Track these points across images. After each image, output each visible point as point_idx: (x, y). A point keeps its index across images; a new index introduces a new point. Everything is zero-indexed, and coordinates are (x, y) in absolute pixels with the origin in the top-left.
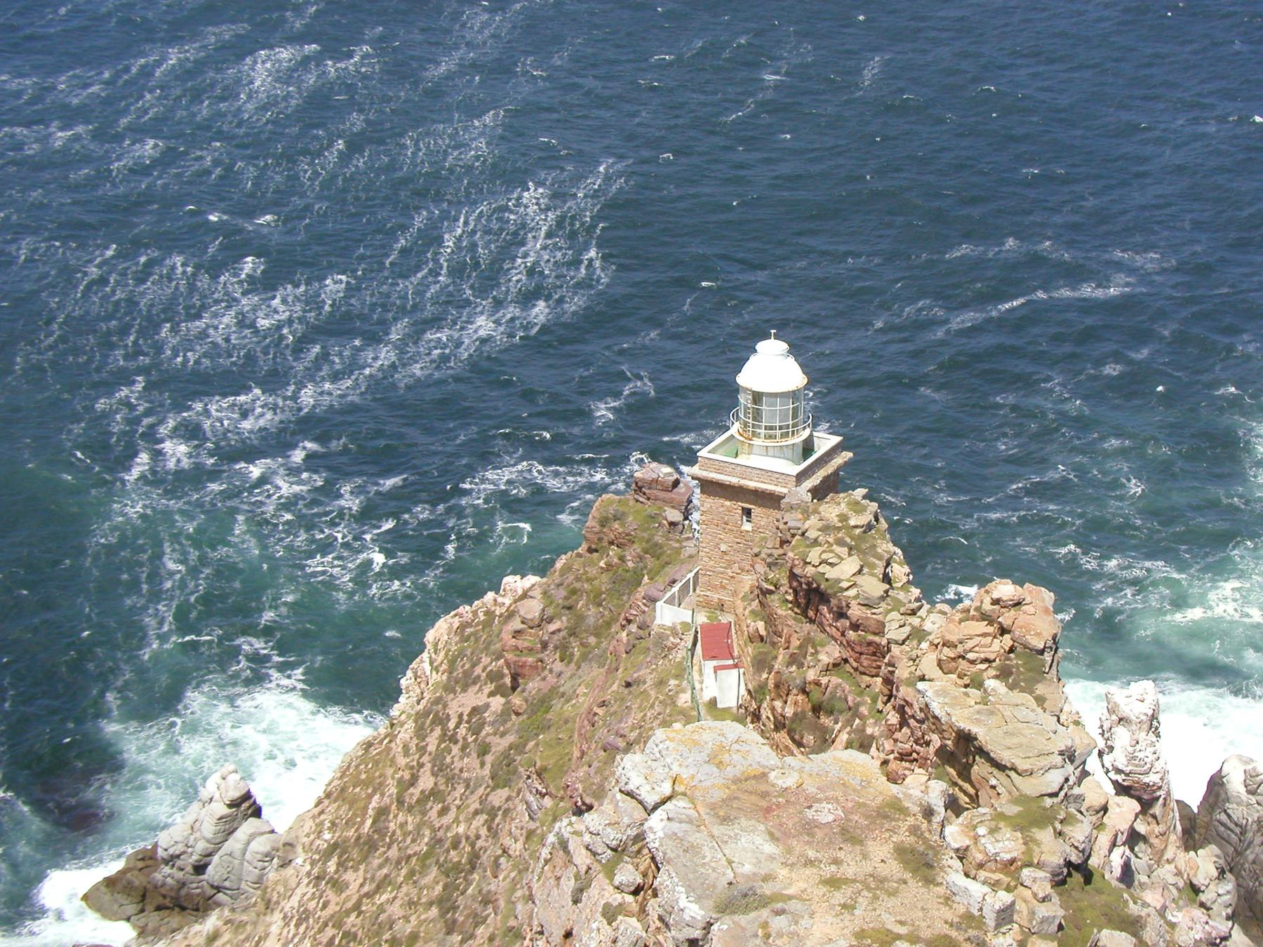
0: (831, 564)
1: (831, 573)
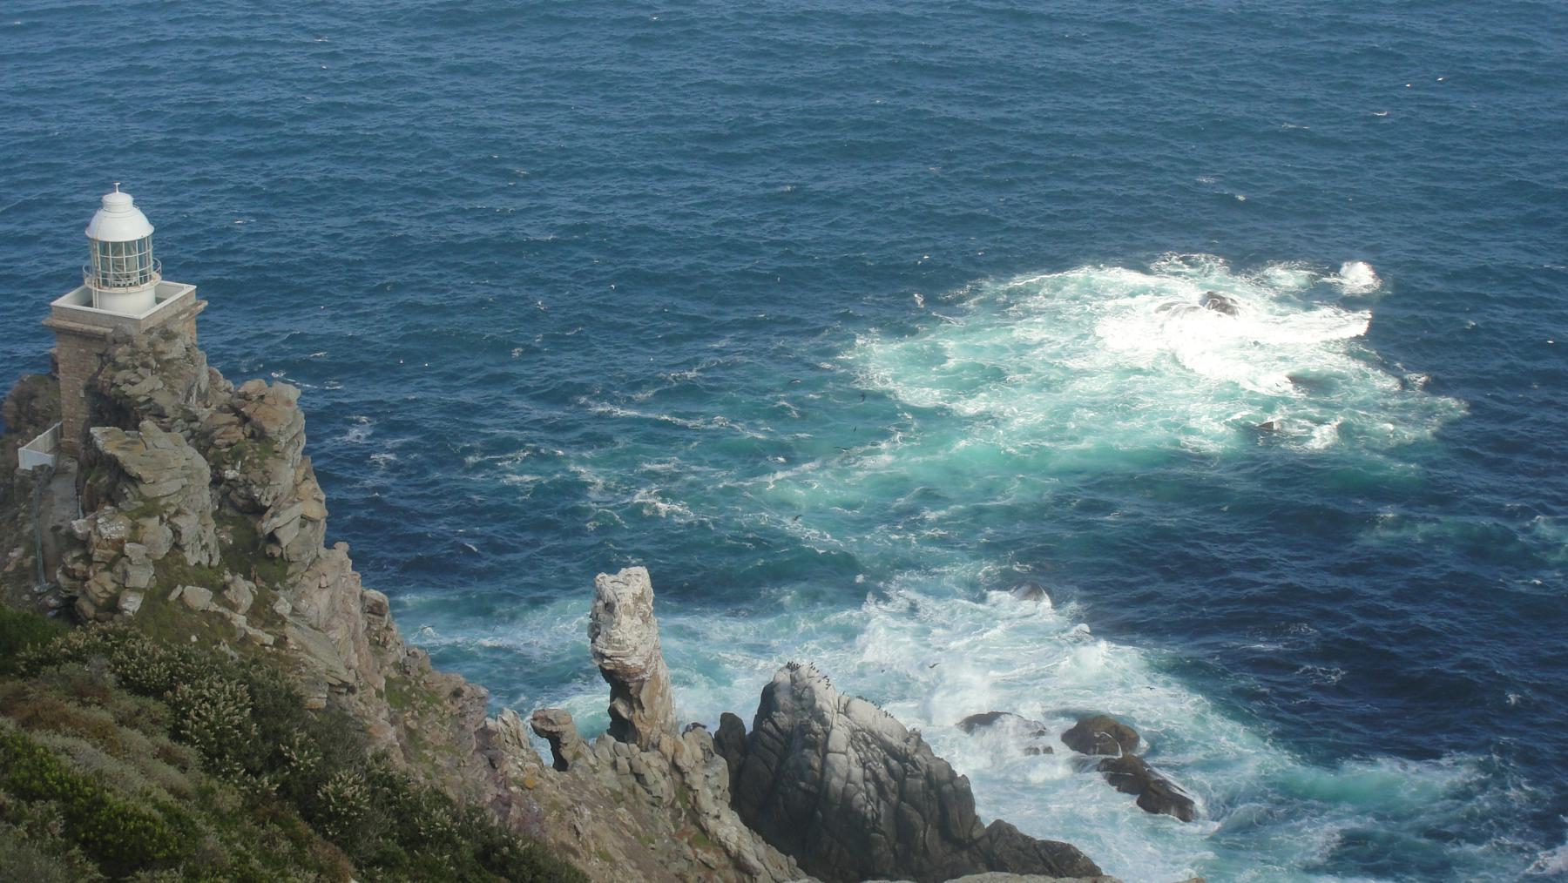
0: (133, 384)
1: (129, 390)
